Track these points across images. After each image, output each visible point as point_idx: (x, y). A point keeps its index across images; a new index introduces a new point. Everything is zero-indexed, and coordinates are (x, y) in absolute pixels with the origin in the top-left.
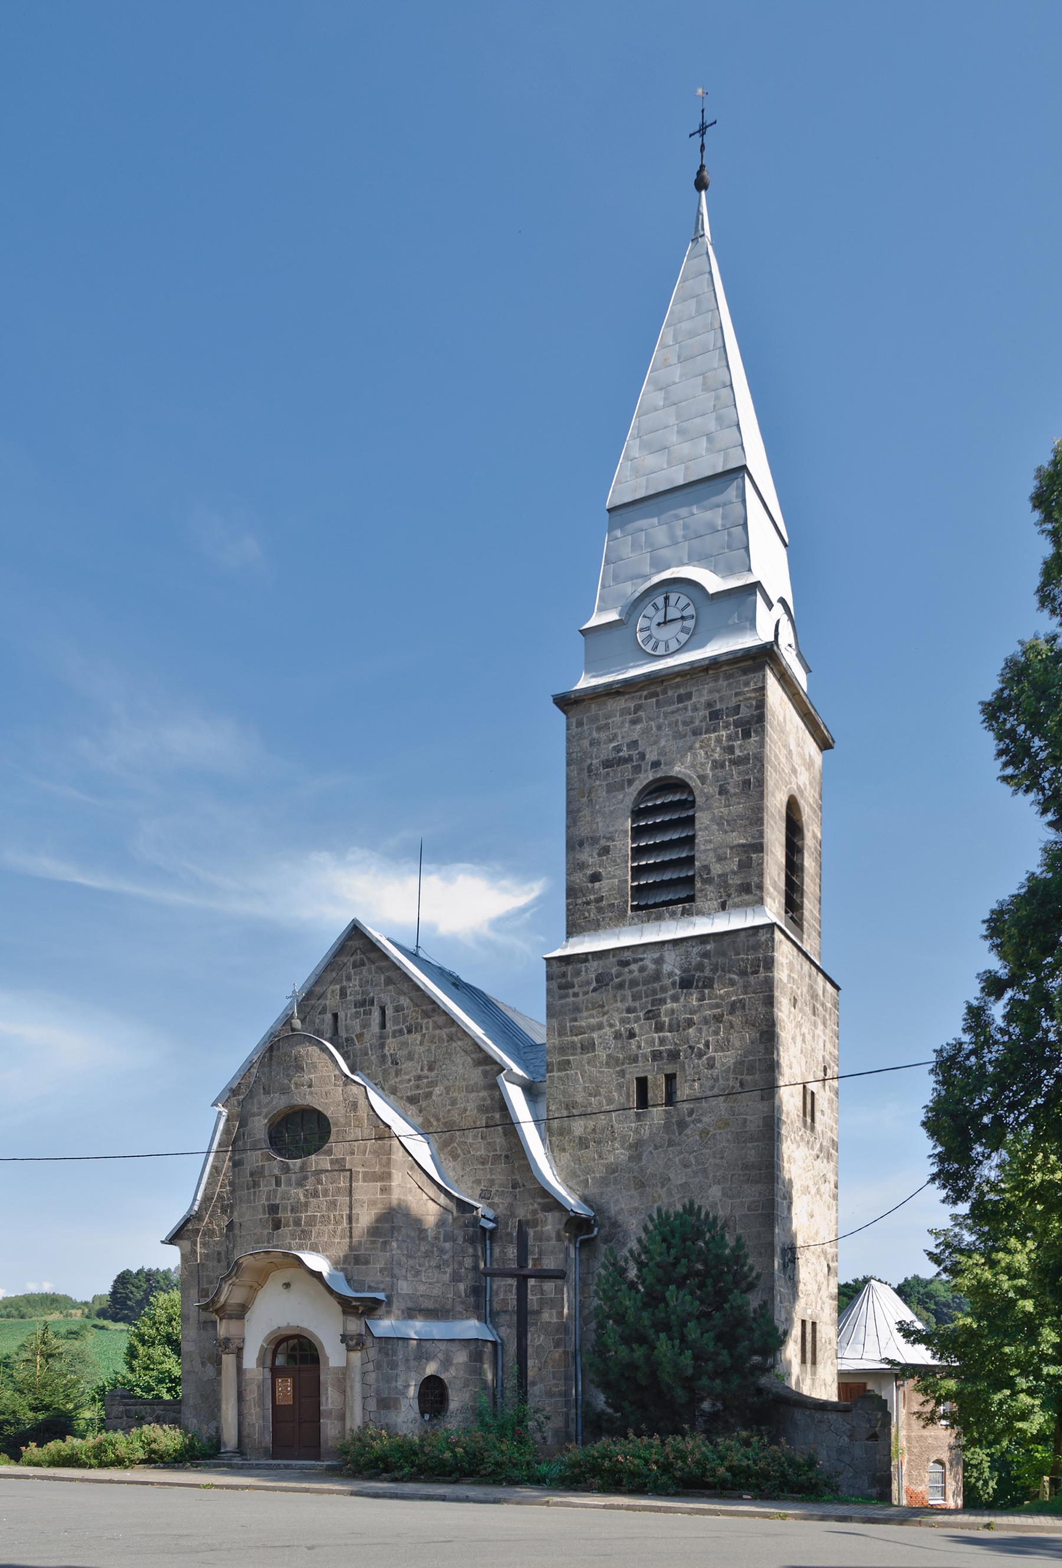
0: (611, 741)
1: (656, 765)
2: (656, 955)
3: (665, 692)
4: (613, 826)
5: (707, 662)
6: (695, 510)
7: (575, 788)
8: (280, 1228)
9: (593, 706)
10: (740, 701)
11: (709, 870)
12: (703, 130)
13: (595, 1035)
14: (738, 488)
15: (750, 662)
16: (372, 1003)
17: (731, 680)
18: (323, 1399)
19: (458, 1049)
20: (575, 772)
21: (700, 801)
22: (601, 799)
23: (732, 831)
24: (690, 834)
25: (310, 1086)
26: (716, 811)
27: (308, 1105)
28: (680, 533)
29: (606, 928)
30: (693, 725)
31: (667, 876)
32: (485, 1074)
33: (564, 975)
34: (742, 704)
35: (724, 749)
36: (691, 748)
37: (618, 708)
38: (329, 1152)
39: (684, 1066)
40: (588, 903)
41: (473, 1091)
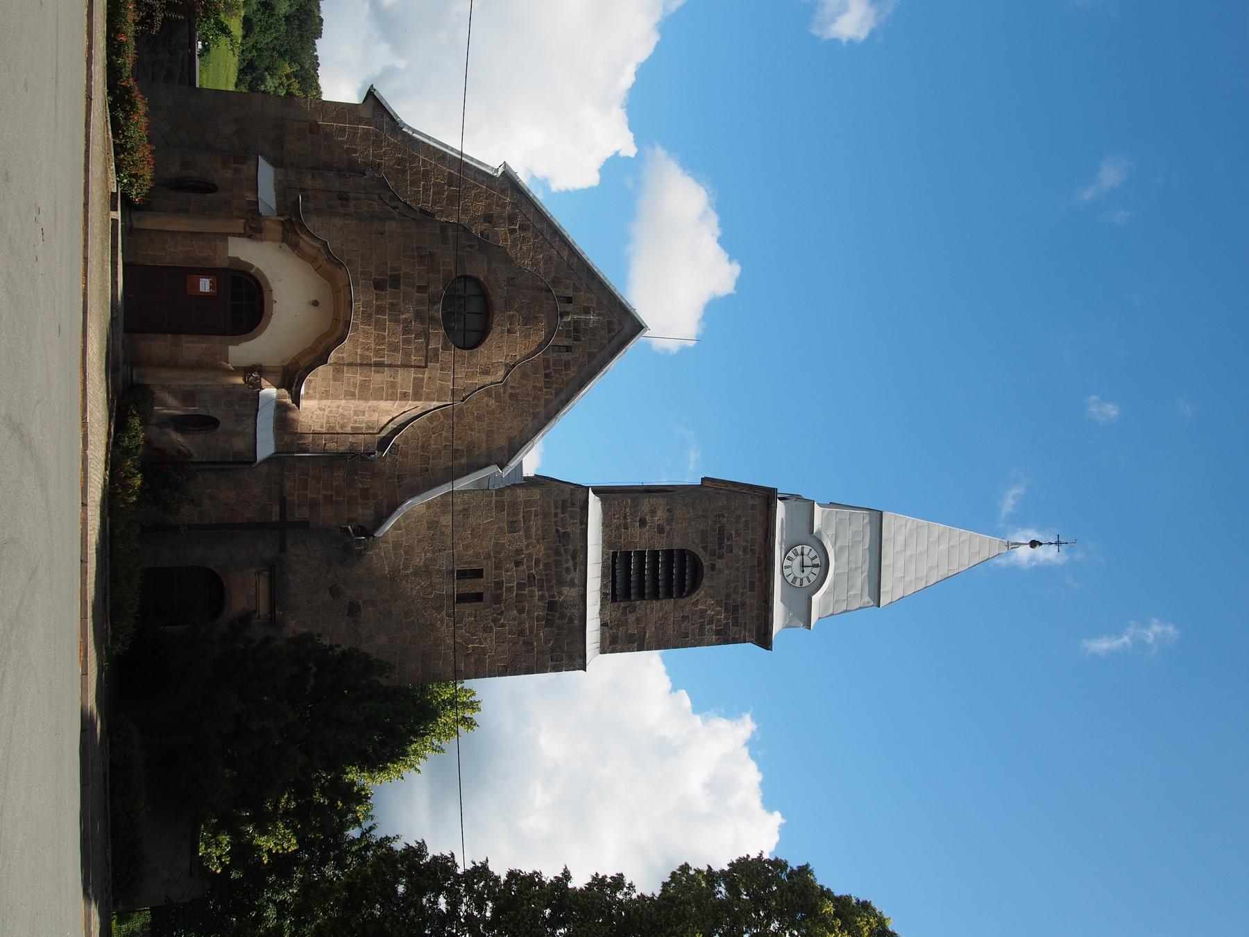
1: (713, 567)
2: (576, 581)
6: (865, 574)
8: (376, 289)
13: (521, 533)
14: (868, 602)
15: (763, 632)
16: (576, 339)
17: (755, 619)
18: (194, 338)
19: (526, 423)
22: (698, 526)
25: (509, 331)
27: (492, 328)
29: (603, 532)
32: (501, 449)
33: (573, 505)
37: (757, 537)
38: (445, 348)
39: (488, 608)
40: (625, 517)
41: (488, 436)
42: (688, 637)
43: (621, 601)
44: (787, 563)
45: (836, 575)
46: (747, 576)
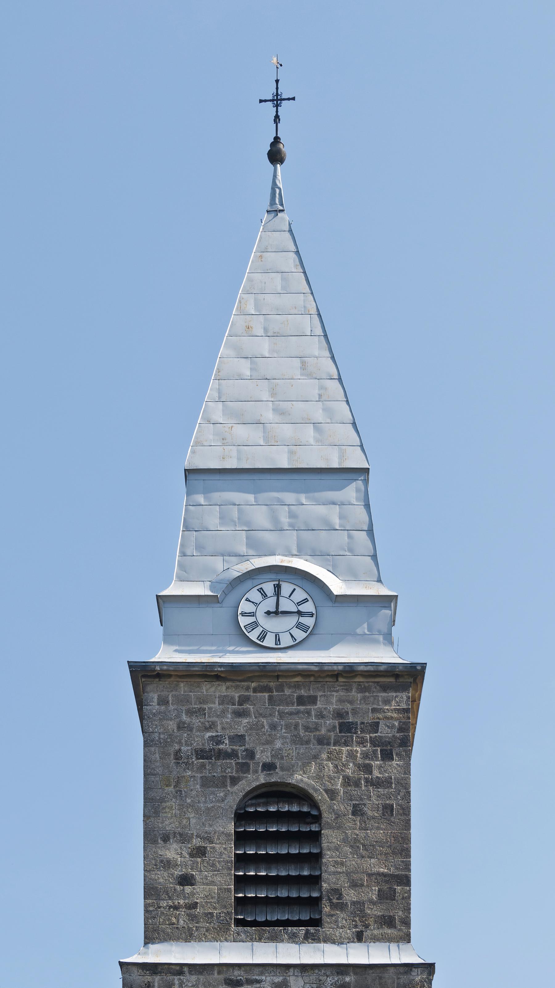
0: (207, 729)
1: (269, 767)
2: (278, 979)
3: (280, 688)
4: (211, 826)
5: (340, 668)
6: (303, 498)
7: (158, 774)
9: (182, 685)
10: (378, 718)
11: (341, 894)
12: (277, 100)
14: (358, 490)
15: (392, 680)
20: (157, 756)
21: (327, 816)
22: (194, 793)
23: (371, 858)
24: (315, 851)
26: (349, 832)
28: (285, 520)
29: (200, 940)
30: (318, 733)
31: (283, 893)
34: (381, 722)
35: (359, 766)
36: (316, 757)
37: (217, 694)
40: (176, 908)
42: (392, 806)
43: (321, 912)
44: (269, 642)
45: (300, 553)
46: (288, 709)
